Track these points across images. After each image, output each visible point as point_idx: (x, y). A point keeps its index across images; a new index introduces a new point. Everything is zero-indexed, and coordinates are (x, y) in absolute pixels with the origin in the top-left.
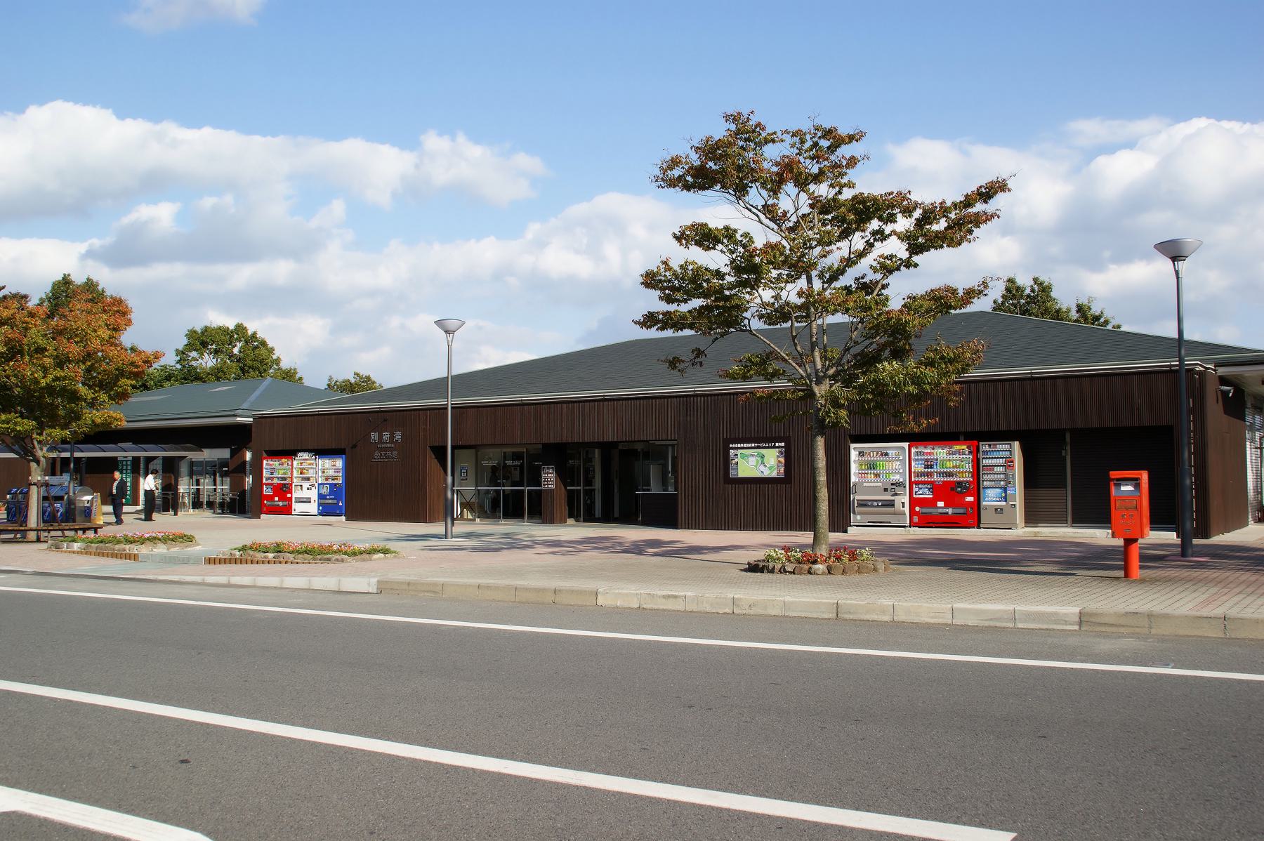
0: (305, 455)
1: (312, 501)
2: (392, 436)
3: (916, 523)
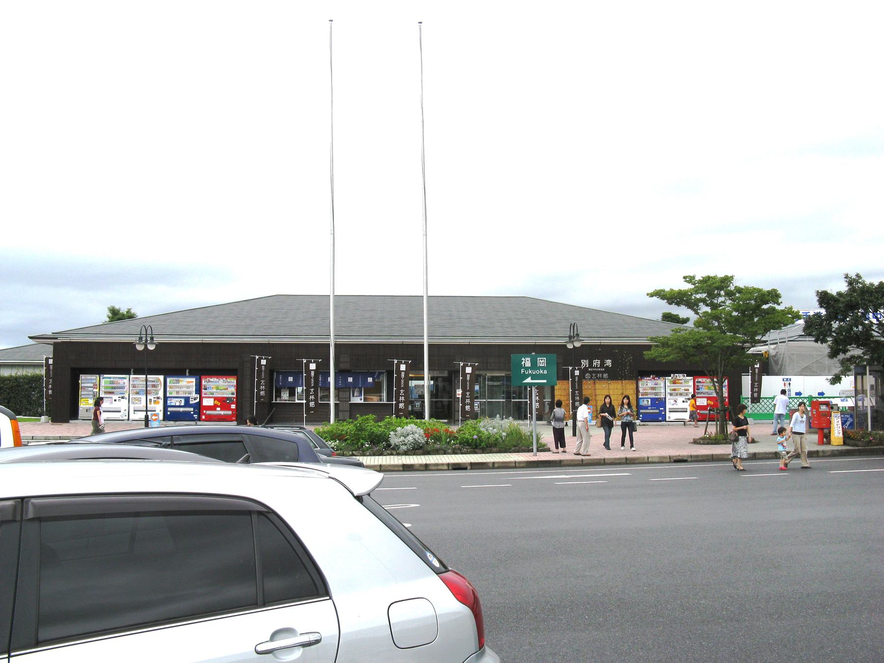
0: (680, 376)
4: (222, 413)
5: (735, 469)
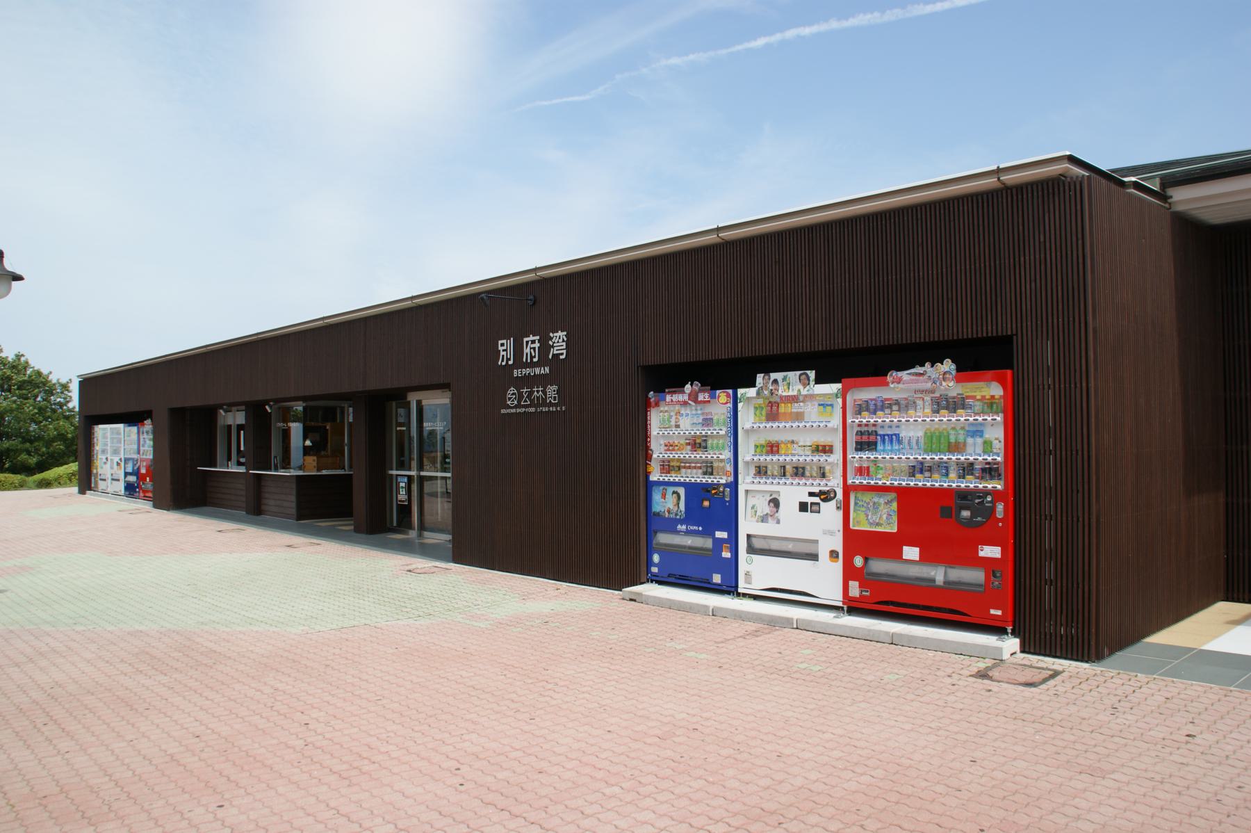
0: (790, 383)
1: (824, 555)
2: (545, 347)
3: (654, 575)
4: (938, 574)
5: (537, 759)
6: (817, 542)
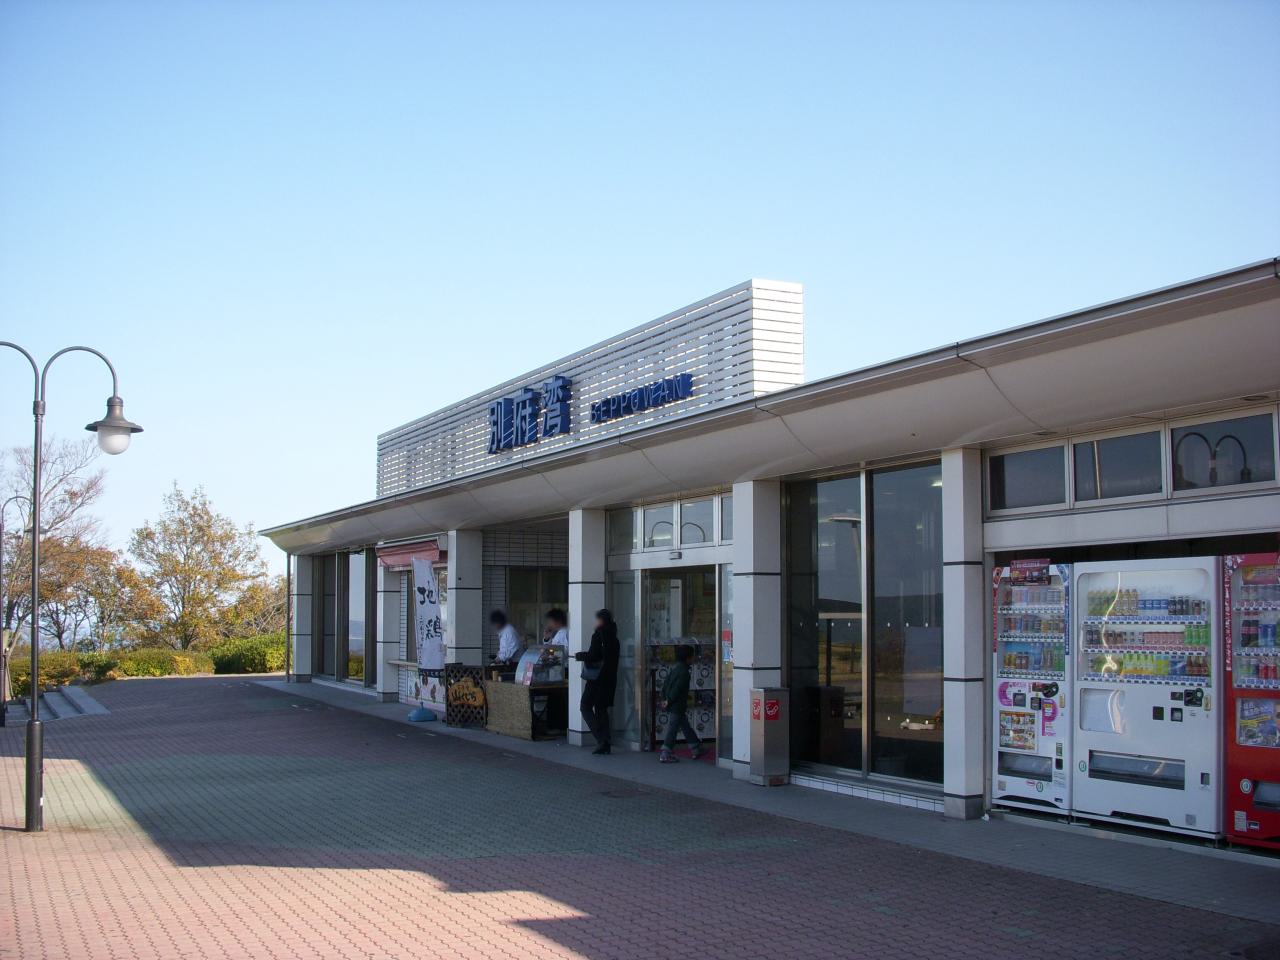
1: (1191, 778)
6: (1184, 761)
